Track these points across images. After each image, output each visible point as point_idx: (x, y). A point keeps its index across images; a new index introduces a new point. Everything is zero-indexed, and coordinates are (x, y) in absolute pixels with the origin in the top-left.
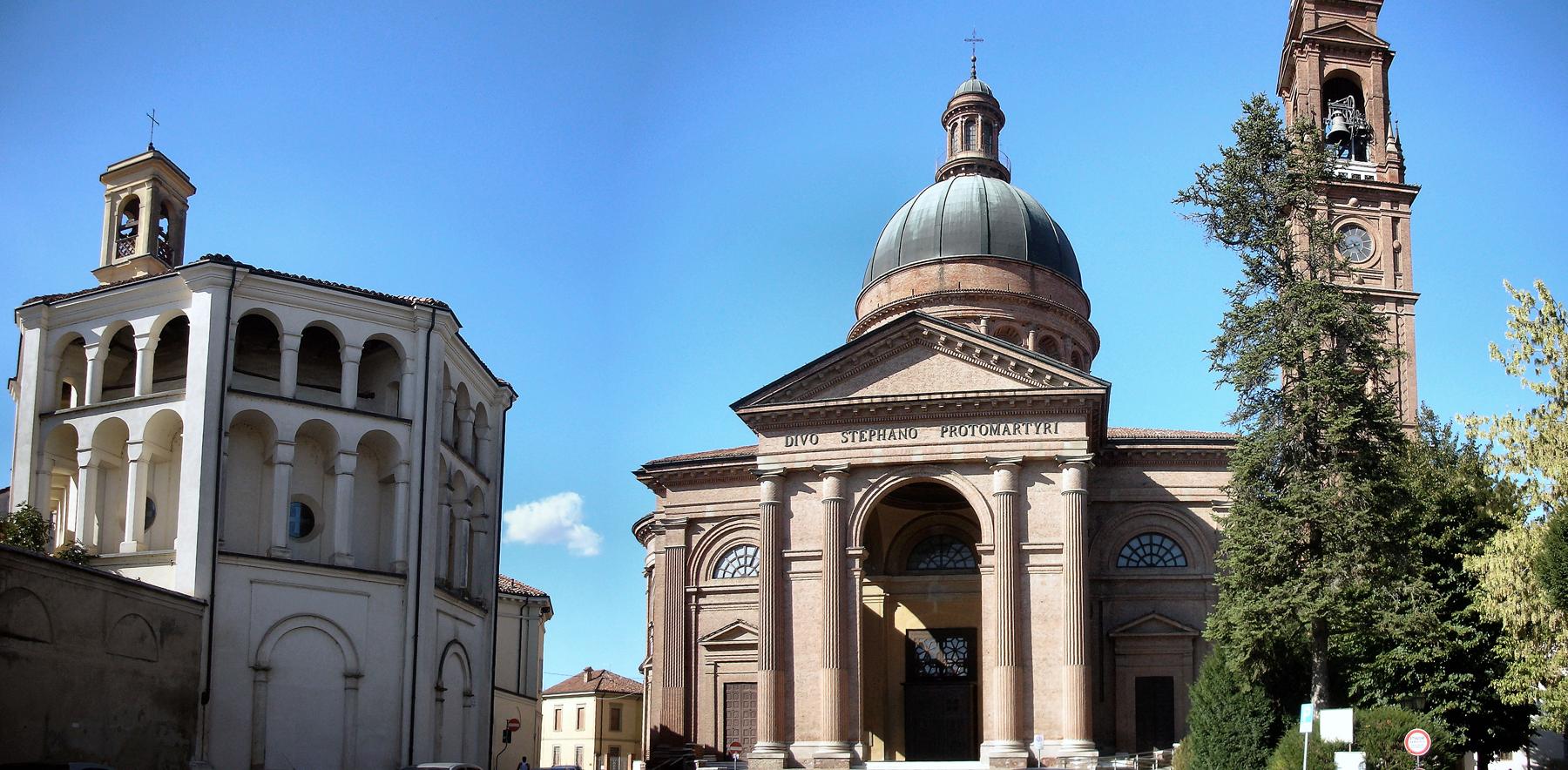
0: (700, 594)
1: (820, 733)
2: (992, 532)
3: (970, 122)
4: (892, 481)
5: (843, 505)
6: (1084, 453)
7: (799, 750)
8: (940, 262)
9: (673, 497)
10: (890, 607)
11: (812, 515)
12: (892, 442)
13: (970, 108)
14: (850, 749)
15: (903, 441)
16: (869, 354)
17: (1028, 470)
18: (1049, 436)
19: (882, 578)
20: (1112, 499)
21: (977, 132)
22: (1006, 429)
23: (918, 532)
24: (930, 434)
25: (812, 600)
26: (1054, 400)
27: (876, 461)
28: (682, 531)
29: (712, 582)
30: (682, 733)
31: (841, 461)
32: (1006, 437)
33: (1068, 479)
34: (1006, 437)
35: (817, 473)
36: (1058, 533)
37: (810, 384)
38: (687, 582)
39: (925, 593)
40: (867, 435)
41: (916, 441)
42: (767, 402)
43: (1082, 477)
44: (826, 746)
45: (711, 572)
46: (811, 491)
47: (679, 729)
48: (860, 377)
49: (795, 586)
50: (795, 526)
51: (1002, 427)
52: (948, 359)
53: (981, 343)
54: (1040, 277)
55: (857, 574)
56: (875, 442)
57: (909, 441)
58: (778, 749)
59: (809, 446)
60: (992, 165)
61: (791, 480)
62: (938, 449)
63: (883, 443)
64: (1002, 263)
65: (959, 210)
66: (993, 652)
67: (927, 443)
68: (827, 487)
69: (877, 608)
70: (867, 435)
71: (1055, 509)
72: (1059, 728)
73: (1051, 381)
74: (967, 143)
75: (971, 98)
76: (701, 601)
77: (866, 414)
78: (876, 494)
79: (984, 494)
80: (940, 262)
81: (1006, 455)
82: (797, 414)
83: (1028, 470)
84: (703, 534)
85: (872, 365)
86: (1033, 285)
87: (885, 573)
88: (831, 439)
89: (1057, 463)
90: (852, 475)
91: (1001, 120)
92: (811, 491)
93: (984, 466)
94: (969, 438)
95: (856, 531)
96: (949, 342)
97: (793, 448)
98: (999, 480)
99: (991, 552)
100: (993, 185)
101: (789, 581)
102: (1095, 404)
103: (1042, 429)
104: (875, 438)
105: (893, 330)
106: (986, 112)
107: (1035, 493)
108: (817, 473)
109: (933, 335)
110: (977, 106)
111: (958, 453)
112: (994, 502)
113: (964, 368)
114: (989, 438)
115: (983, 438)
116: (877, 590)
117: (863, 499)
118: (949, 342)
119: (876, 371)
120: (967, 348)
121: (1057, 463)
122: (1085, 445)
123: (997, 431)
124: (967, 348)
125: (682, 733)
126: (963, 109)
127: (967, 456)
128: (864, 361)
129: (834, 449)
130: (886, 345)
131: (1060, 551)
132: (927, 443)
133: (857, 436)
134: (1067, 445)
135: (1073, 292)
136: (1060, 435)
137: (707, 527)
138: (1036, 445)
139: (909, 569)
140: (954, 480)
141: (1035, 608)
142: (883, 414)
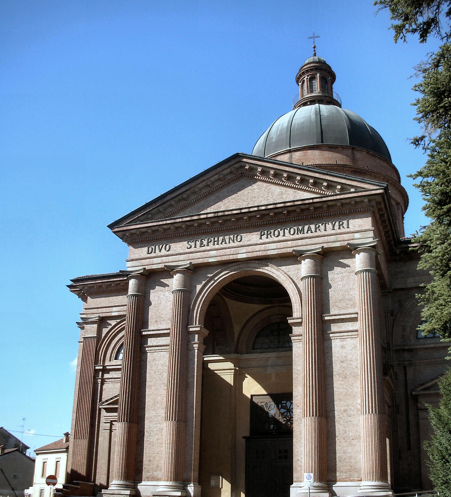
0: (105, 370)
1: (159, 474)
2: (301, 309)
3: (312, 79)
4: (224, 275)
5: (186, 297)
6: (371, 240)
7: (144, 487)
8: (290, 151)
9: (92, 302)
10: (239, 377)
11: (163, 303)
12: (224, 245)
13: (311, 70)
14: (183, 488)
15: (232, 244)
16: (208, 186)
17: (326, 258)
18: (342, 230)
19: (234, 356)
20: (409, 286)
21: (317, 84)
22: (309, 229)
23: (246, 314)
24: (252, 237)
25: (160, 365)
26: (343, 203)
27: (211, 260)
28: (95, 326)
29: (114, 362)
30: (84, 474)
31: (184, 262)
32: (310, 234)
33: (359, 261)
34: (310, 234)
35: (168, 272)
36: (354, 305)
37: (165, 209)
38: (96, 362)
39: (266, 367)
40: (205, 242)
41: (241, 243)
42: (134, 222)
43: (371, 259)
44: (164, 485)
45: (114, 355)
46: (165, 285)
47: (83, 471)
48: (202, 202)
49: (150, 356)
50: (152, 312)
51: (306, 228)
52: (265, 184)
53: (287, 169)
54: (358, 155)
55: (196, 346)
56: (211, 246)
57: (237, 244)
58: (126, 487)
59: (164, 252)
60: (328, 99)
61: (151, 278)
62: (257, 248)
63: (217, 246)
64: (331, 148)
65: (302, 121)
66: (301, 406)
67: (250, 244)
68: (176, 282)
69: (229, 378)
70: (205, 242)
71: (350, 286)
72: (358, 471)
73: (342, 189)
74: (311, 90)
75: (314, 65)
76: (106, 376)
77: (204, 227)
78: (212, 285)
79: (294, 278)
80: (290, 151)
81: (309, 248)
82: (154, 230)
83: (326, 258)
84: (110, 327)
85: (210, 194)
86: (354, 160)
87: (236, 352)
88: (179, 247)
89: (349, 251)
90: (194, 271)
91: (333, 77)
92: (165, 285)
93: (294, 258)
94: (281, 238)
95: (197, 313)
96: (265, 172)
97: (153, 255)
98: (305, 267)
99: (299, 324)
100: (325, 109)
101: (146, 353)
102: (378, 203)
103: (336, 227)
104: (211, 244)
105: (223, 167)
106: (324, 73)
107: (335, 276)
108: (168, 272)
109: (252, 169)
110: (316, 69)
111: (273, 249)
112: (301, 285)
113: (276, 190)
114: (296, 236)
115: (292, 237)
116: (230, 365)
117: (203, 290)
118: (265, 172)
119: (213, 197)
120: (277, 175)
121: (349, 251)
122: (371, 234)
123: (302, 231)
124: (277, 175)
125: (84, 474)
126: (307, 71)
127: (280, 251)
128: (204, 191)
129: (181, 253)
130: (219, 179)
131: (355, 320)
132: (250, 244)
133: (198, 243)
134: (357, 235)
135: (385, 164)
136: (352, 228)
137: (113, 323)
138: (332, 238)
139: (253, 349)
140: (271, 271)
141: (337, 367)
142: (217, 225)
